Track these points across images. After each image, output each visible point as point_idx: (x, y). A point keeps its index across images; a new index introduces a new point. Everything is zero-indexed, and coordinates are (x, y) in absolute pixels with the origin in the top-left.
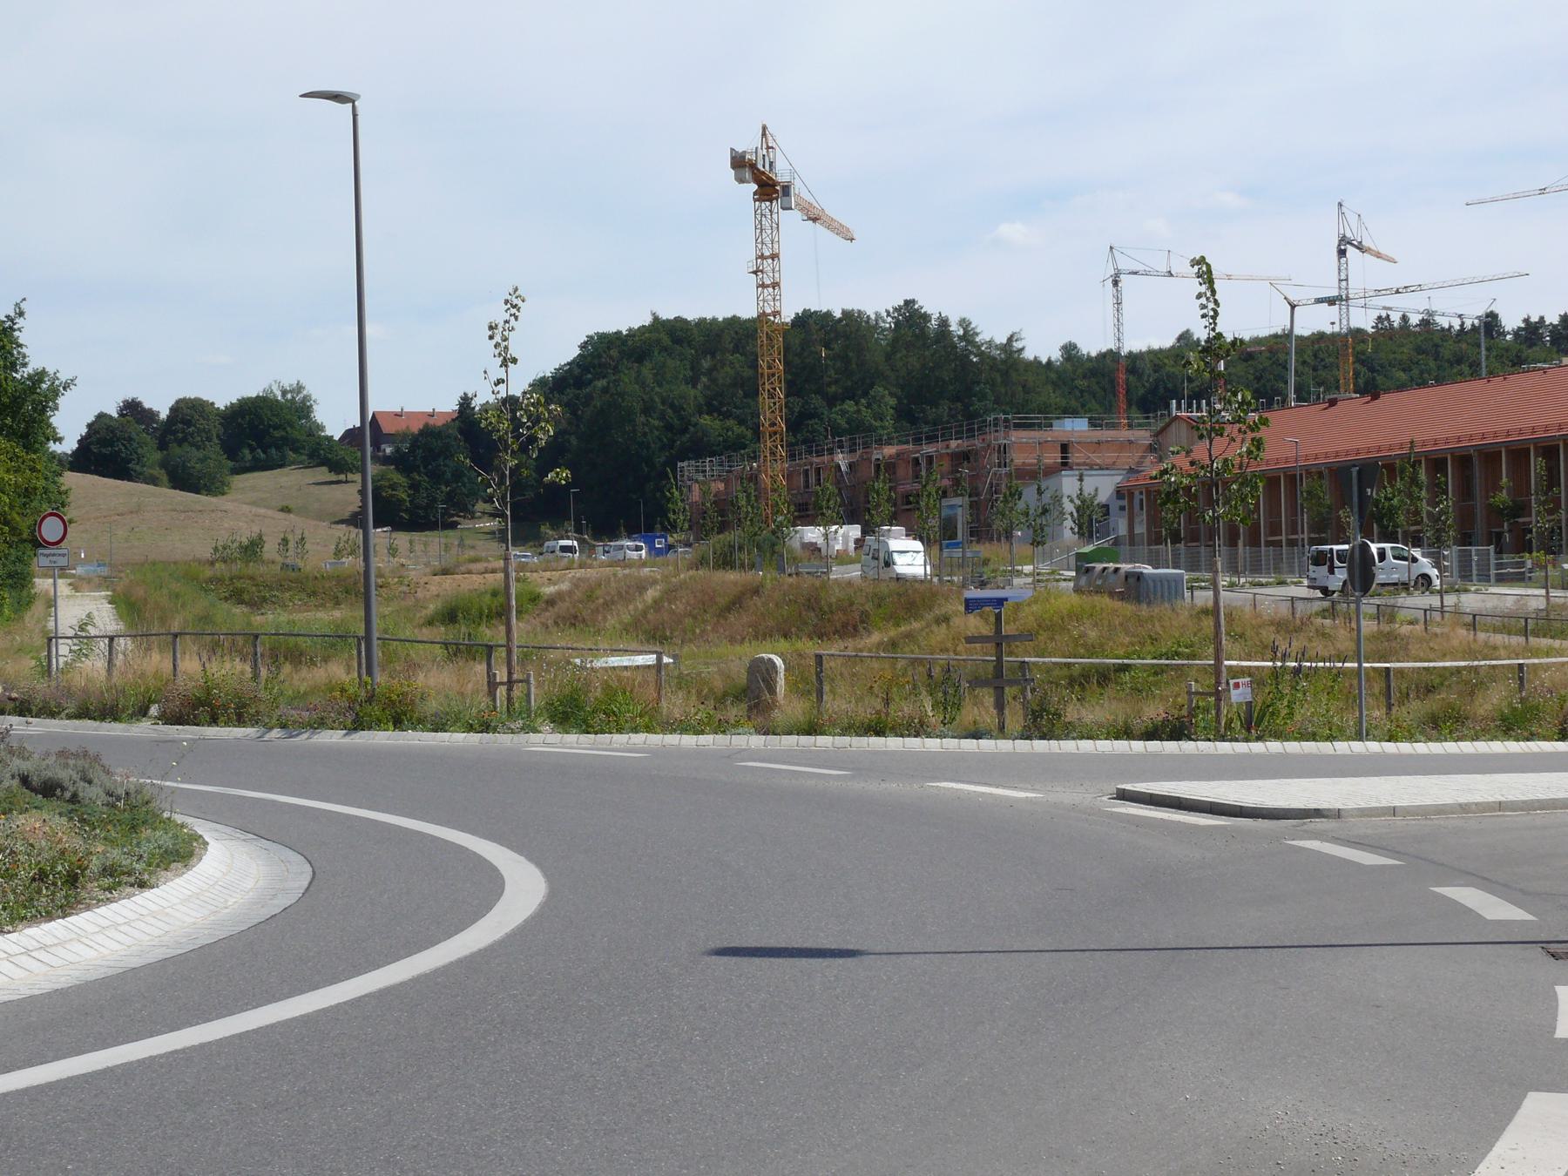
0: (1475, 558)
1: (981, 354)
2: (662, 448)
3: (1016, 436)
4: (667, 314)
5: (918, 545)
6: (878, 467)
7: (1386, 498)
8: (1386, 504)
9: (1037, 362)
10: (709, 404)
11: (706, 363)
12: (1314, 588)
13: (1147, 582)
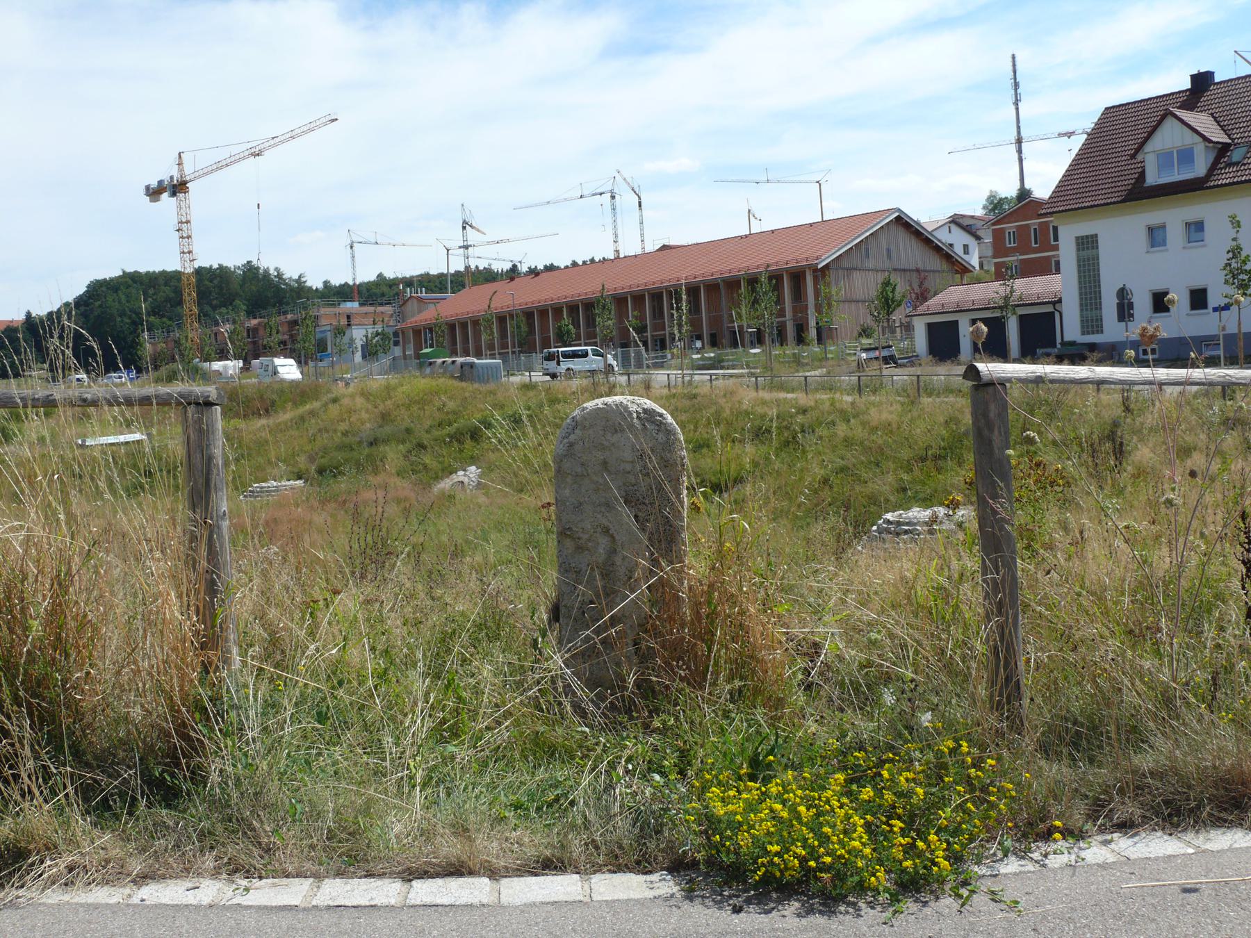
1: (286, 284)
2: (131, 333)
3: (323, 311)
4: (130, 269)
5: (291, 361)
6: (248, 331)
9: (310, 288)
10: (153, 311)
11: (151, 292)
12: (547, 375)
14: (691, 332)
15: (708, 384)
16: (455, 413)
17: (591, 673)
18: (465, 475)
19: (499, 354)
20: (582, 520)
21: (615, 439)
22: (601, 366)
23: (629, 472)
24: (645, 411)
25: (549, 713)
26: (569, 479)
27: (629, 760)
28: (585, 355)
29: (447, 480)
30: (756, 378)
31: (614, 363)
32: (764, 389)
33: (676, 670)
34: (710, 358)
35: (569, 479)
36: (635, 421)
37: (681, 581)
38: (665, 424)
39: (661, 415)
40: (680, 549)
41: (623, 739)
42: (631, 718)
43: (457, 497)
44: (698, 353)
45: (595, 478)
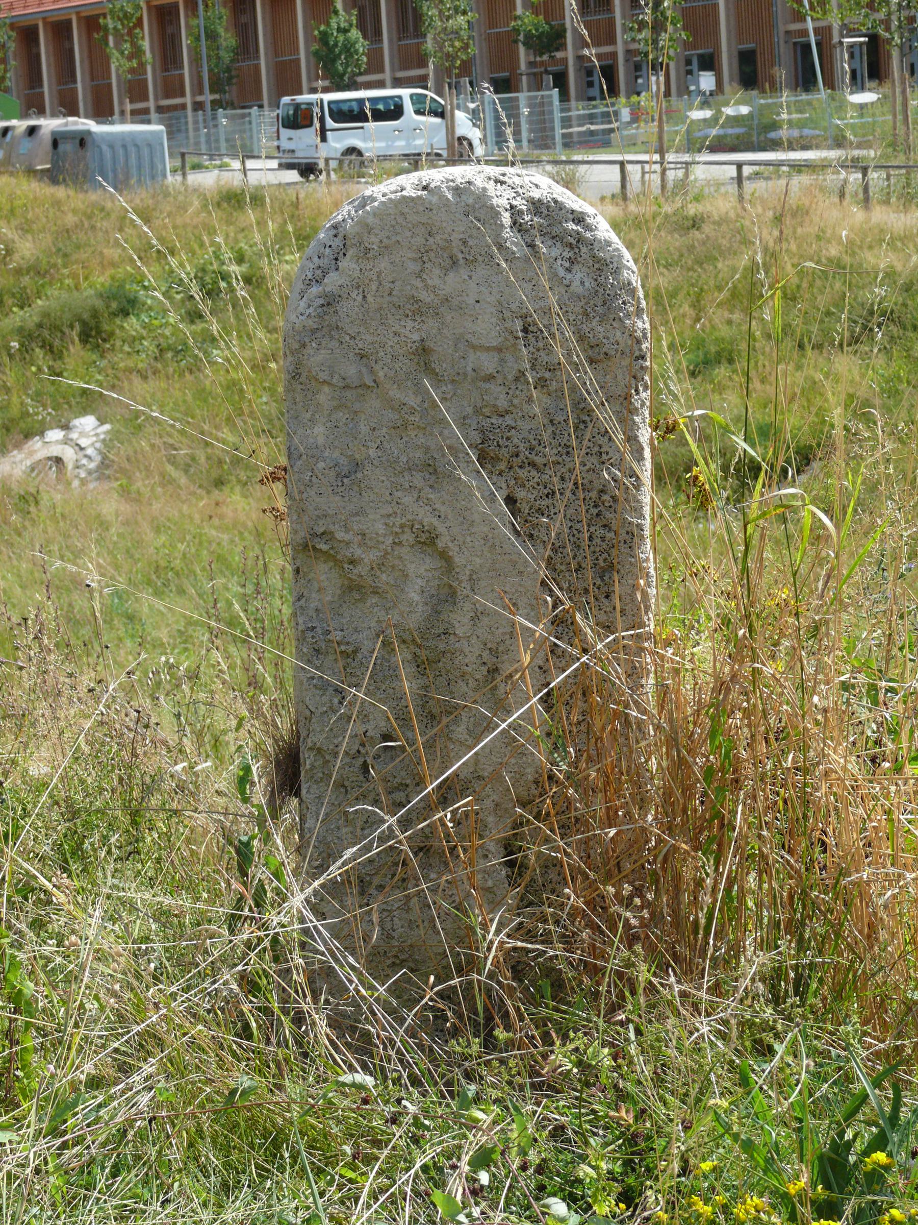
0: (526, 111)
7: (339, 30)
8: (341, 38)
12: (290, 166)
13: (98, 147)
14: (686, 45)
15: (733, 189)
16: (35, 270)
17: (387, 935)
18: (66, 441)
19: (160, 109)
20: (360, 512)
21: (452, 282)
22: (440, 142)
23: (490, 378)
24: (537, 206)
25: (268, 1042)
26: (324, 397)
27: (483, 1159)
28: (394, 112)
29: (17, 455)
30: (865, 171)
31: (475, 135)
32: (887, 202)
33: (615, 908)
34: (736, 120)
35: (324, 397)
36: (507, 233)
37: (634, 674)
38: (591, 244)
39: (579, 218)
40: (635, 587)
41: (466, 1104)
42: (490, 1043)
43: (45, 499)
44: (705, 104)
45: (395, 393)
